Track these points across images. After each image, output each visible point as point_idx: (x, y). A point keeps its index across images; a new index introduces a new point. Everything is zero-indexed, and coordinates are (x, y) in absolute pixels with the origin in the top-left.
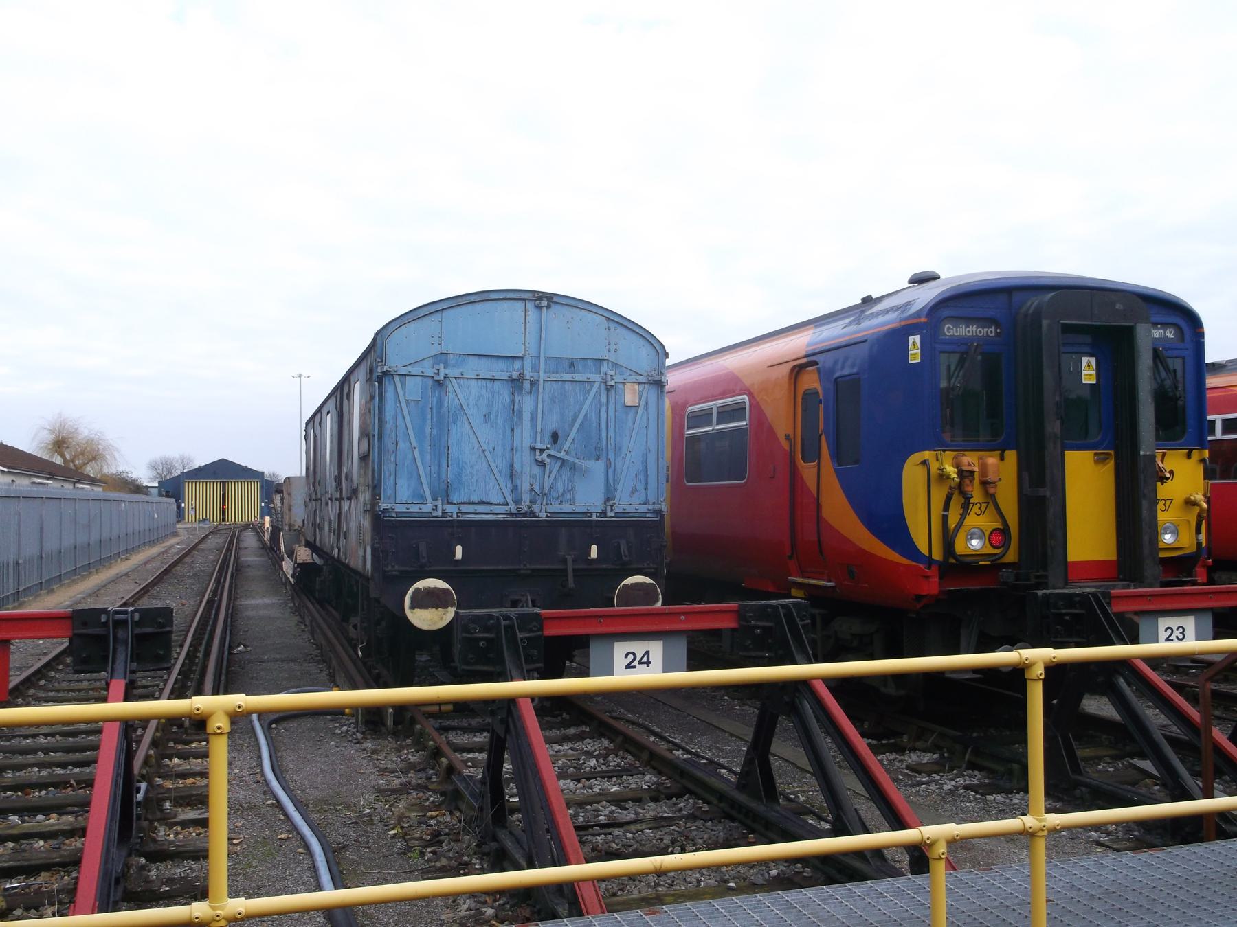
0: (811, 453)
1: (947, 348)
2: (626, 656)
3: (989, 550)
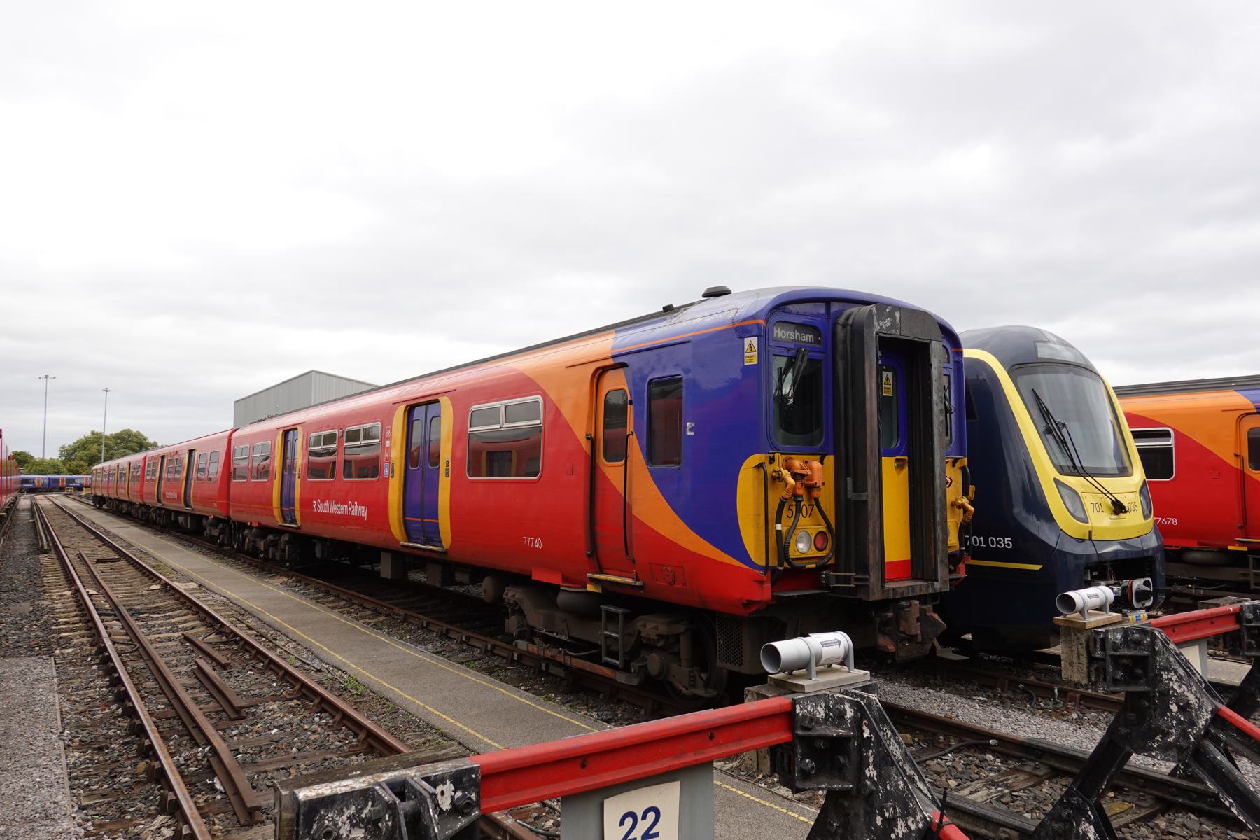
0: (617, 450)
1: (777, 351)
2: (622, 823)
3: (814, 553)
